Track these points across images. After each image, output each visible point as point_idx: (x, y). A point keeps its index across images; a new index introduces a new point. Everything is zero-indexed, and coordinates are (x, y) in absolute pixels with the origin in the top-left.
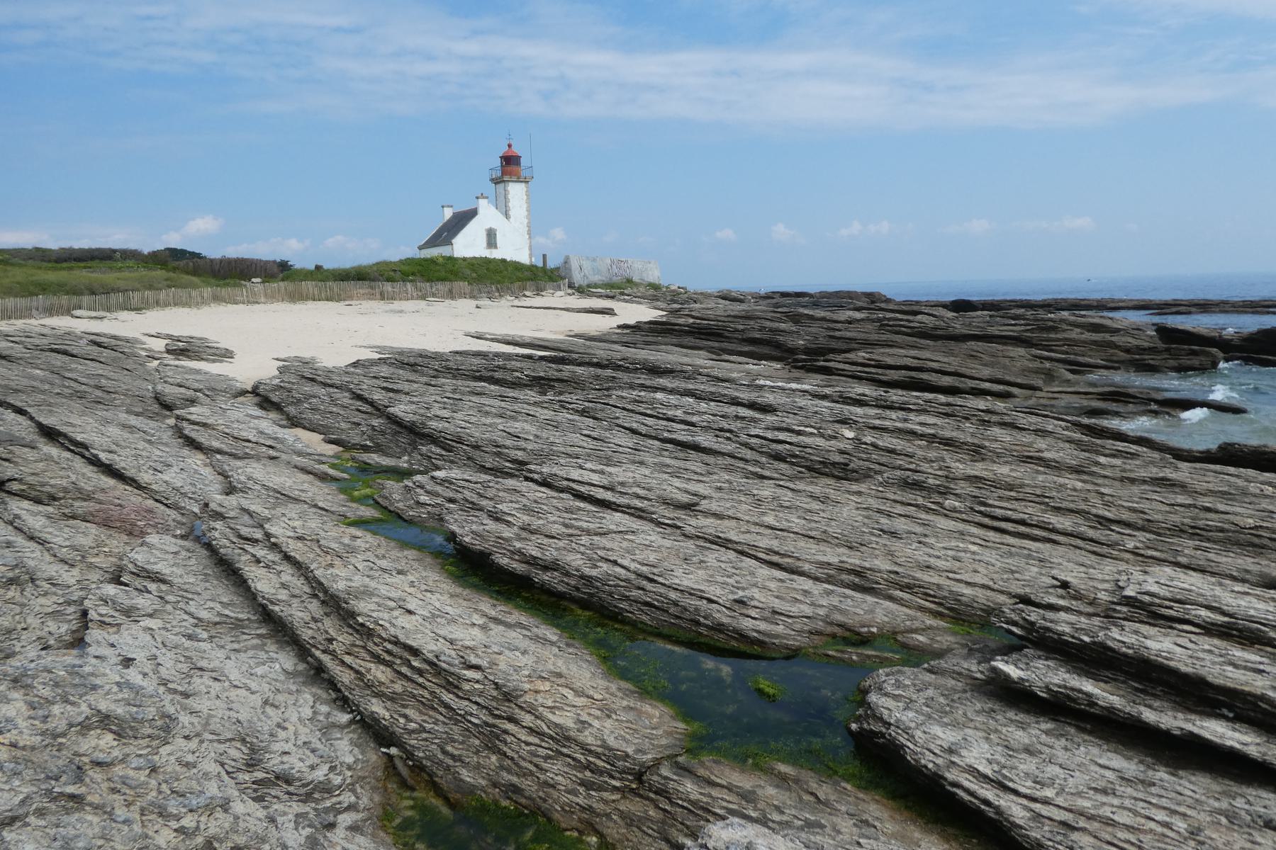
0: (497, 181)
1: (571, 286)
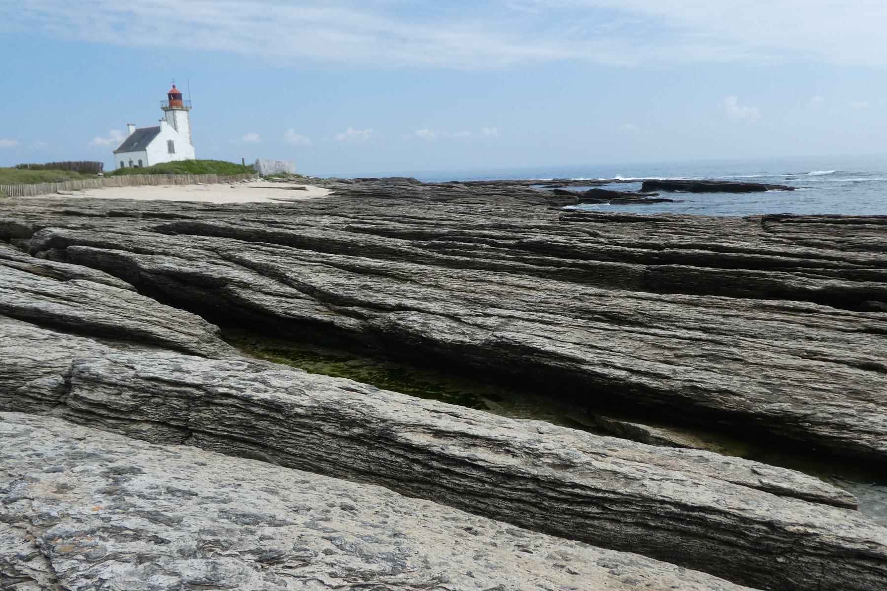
0: (166, 109)
1: (261, 176)
